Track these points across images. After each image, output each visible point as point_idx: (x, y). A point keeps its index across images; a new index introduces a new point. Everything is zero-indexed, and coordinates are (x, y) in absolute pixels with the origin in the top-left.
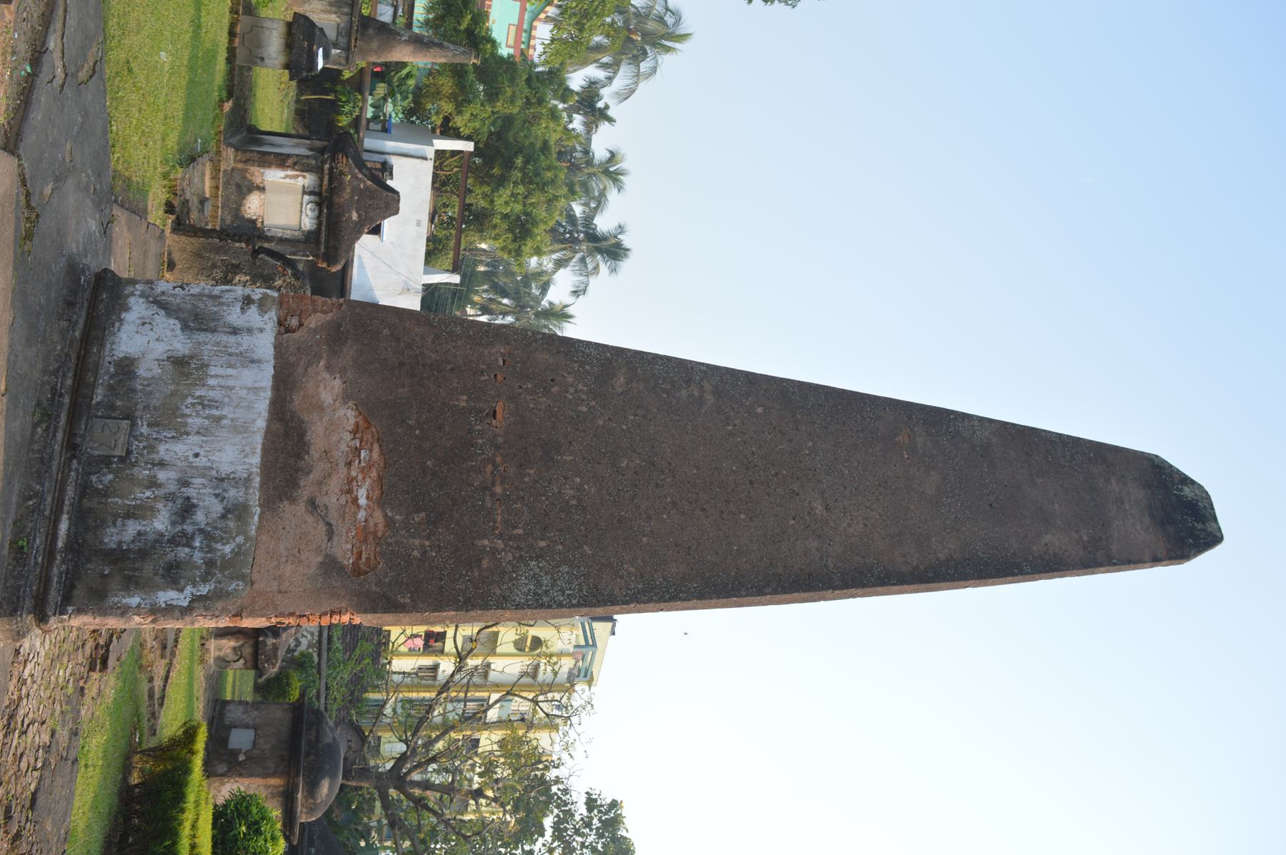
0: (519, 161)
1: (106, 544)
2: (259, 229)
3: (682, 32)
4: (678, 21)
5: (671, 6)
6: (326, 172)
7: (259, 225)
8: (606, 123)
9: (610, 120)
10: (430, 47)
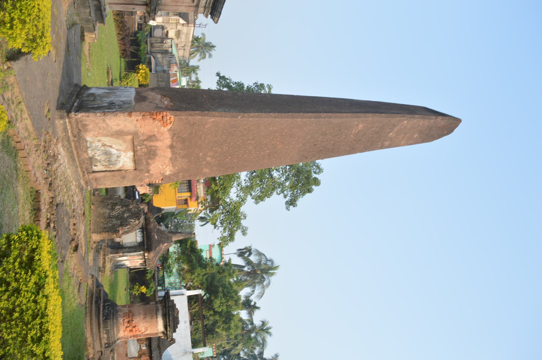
0: (220, 289)
2: (121, 245)
3: (275, 266)
4: (273, 263)
5: (268, 259)
7: (121, 244)
8: (257, 310)
9: (258, 308)
10: (176, 234)
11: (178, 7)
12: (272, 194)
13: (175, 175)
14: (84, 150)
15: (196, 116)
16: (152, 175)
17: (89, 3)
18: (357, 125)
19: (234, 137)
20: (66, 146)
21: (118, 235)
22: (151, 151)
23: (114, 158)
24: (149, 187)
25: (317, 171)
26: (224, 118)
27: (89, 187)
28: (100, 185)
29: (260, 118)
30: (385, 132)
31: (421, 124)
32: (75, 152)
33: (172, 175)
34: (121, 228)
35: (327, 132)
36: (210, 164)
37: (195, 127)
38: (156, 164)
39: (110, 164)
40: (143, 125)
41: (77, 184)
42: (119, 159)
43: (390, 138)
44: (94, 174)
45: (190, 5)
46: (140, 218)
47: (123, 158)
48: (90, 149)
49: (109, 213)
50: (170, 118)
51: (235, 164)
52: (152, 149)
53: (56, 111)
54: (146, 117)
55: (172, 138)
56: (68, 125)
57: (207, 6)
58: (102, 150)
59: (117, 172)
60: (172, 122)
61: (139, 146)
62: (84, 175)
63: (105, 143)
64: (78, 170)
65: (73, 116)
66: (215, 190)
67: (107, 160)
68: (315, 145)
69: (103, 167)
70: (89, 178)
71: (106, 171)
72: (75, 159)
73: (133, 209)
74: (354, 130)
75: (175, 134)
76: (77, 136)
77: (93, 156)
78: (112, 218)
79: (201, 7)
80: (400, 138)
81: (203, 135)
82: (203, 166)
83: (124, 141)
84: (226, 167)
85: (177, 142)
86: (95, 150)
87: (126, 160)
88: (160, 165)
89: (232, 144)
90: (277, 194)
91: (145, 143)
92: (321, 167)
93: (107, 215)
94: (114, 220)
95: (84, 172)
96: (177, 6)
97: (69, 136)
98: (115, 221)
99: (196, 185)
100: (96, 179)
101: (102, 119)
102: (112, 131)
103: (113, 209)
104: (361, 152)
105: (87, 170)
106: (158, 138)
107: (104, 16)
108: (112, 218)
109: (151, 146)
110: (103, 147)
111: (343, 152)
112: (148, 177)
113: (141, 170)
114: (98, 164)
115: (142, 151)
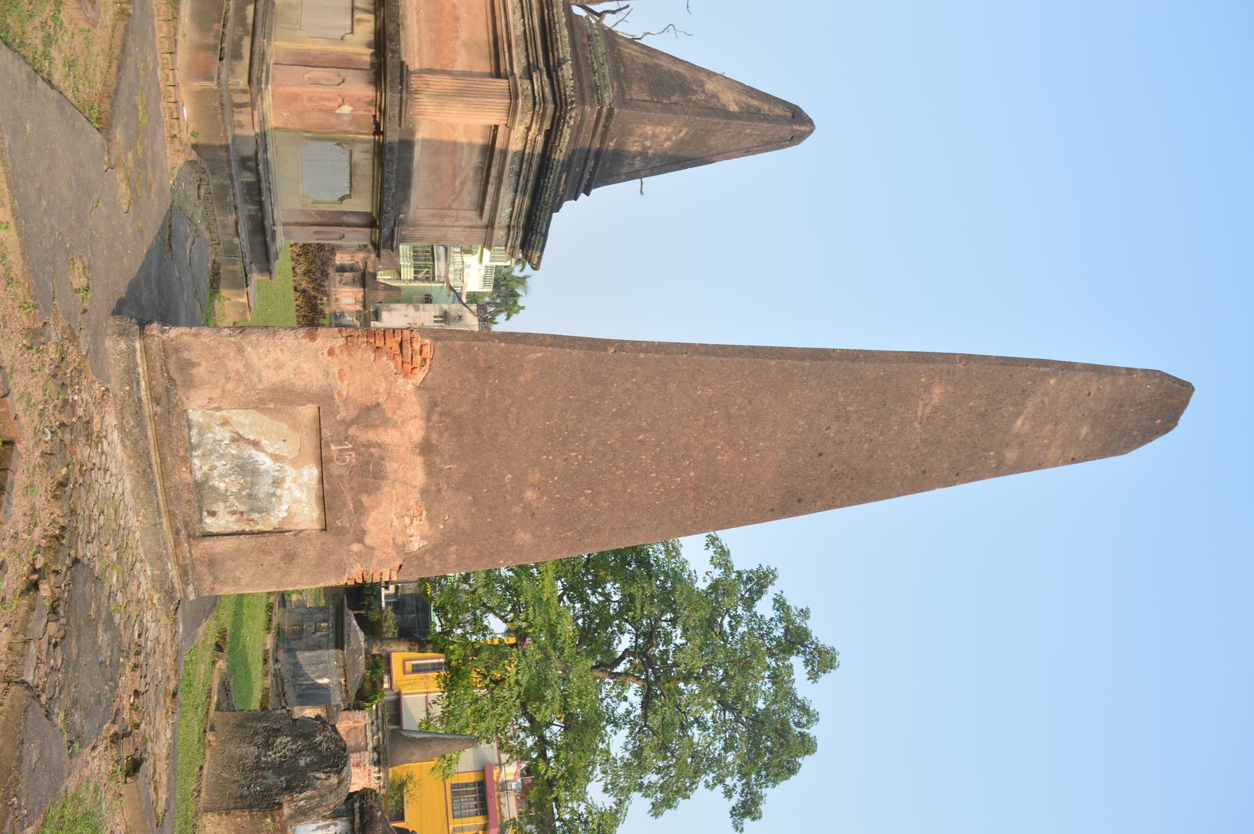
1: (686, 125)
6: (357, 810)
11: (446, 229)
12: (694, 786)
13: (437, 553)
14: (182, 453)
15: (494, 342)
16: (372, 548)
17: (234, 194)
18: (928, 389)
19: (598, 419)
20: (131, 433)
21: (278, 819)
22: (368, 463)
23: (264, 488)
24: (376, 769)
25: (804, 720)
26: (568, 350)
27: (191, 588)
28: (224, 583)
29: (666, 353)
30: (1003, 417)
31: (1093, 389)
32: (154, 458)
33: (426, 552)
34: (287, 797)
35: (848, 408)
36: (533, 515)
37: (491, 381)
38: (381, 509)
39: (252, 510)
40: (346, 369)
41: (157, 572)
42: (279, 492)
43: (1017, 435)
44: (207, 543)
45: (473, 223)
46: (342, 769)
47: (289, 489)
48: (199, 452)
49: (256, 757)
50: (422, 346)
51: (605, 516)
52: (371, 455)
53: (111, 318)
54: (355, 340)
55: (428, 419)
56: (139, 361)
57: (512, 223)
58: (233, 455)
59: (273, 538)
60: (428, 361)
61: (333, 442)
62: (177, 544)
63: (241, 432)
64: (161, 524)
65: (155, 332)
66: (546, 777)
67: (244, 493)
68: (821, 455)
69: (234, 517)
70: (191, 555)
71: (243, 533)
72: (153, 481)
73: (325, 745)
74: (921, 403)
75: (435, 404)
76: (164, 401)
77: (207, 477)
78: (263, 769)
79: (499, 228)
80: (1044, 438)
81: (513, 409)
82: (514, 521)
83: (295, 427)
84: (579, 527)
85: (441, 433)
86: (213, 457)
87: (298, 494)
88: (393, 516)
89: (593, 442)
90: (707, 786)
91: (352, 431)
92: (811, 709)
93: (249, 762)
94: (269, 774)
95: (177, 532)
96: (444, 226)
97: (140, 399)
98: (271, 779)
99: (499, 797)
100: (212, 562)
101: (235, 343)
102: (260, 386)
103: (268, 745)
104: (947, 482)
105: (186, 526)
106: (389, 415)
107: (272, 257)
108: (263, 769)
109: (369, 444)
110: (233, 446)
111: (898, 483)
112: (359, 555)
113: (340, 532)
114: (219, 507)
115: (344, 461)
